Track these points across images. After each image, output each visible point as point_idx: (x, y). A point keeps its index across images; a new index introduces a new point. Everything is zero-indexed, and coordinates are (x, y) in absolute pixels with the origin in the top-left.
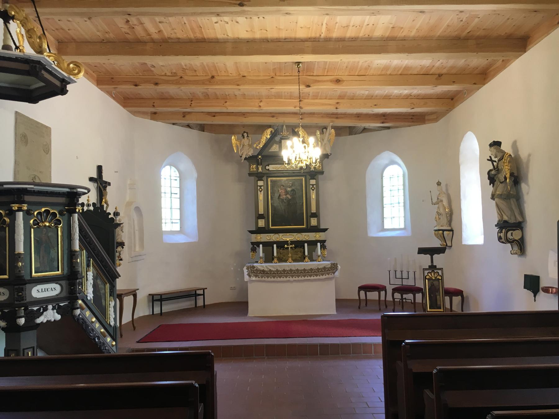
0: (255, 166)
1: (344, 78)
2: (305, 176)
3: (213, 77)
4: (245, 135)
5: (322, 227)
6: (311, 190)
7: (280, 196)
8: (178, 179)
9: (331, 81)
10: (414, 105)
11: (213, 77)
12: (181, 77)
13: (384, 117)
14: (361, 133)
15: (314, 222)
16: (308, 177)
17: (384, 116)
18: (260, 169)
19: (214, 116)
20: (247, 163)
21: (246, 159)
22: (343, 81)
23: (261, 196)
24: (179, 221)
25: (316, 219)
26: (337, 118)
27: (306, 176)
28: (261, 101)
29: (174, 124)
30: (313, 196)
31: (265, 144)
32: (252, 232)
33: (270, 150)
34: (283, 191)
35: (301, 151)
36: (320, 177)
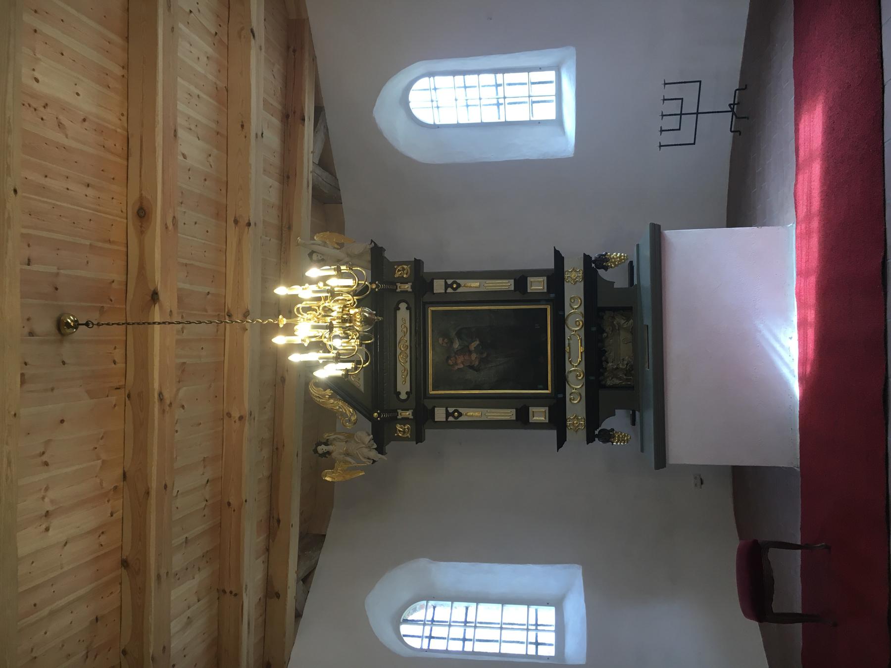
0: (398, 427)
1: (134, 196)
2: (425, 304)
3: (125, 563)
4: (322, 449)
5: (550, 265)
6: (459, 290)
7: (471, 367)
8: (431, 603)
9: (141, 232)
10: (242, 29)
11: (125, 563)
12: (124, 652)
13: (290, 118)
14: (333, 174)
15: (537, 285)
16: (427, 298)
17: (287, 116)
18: (408, 414)
19: (279, 521)
20: (390, 447)
21: (380, 450)
22: (141, 198)
23: (472, 414)
24: (533, 609)
25: (530, 279)
26: (290, 228)
27: (425, 304)
28: (229, 415)
29: (298, 615)
30: (474, 285)
31: (345, 401)
32: (561, 441)
33: (362, 388)
34: (460, 359)
35: (316, 324)
36: (427, 268)
